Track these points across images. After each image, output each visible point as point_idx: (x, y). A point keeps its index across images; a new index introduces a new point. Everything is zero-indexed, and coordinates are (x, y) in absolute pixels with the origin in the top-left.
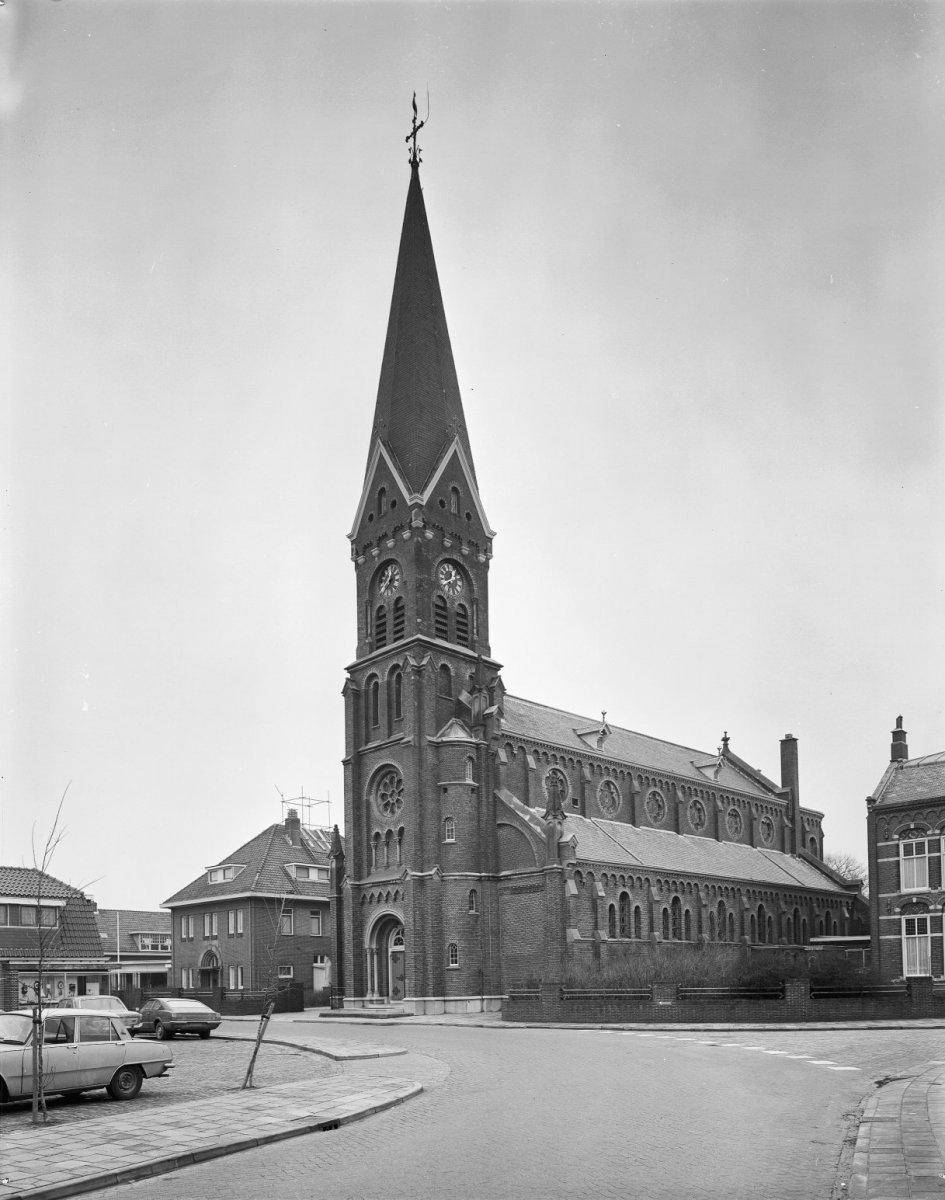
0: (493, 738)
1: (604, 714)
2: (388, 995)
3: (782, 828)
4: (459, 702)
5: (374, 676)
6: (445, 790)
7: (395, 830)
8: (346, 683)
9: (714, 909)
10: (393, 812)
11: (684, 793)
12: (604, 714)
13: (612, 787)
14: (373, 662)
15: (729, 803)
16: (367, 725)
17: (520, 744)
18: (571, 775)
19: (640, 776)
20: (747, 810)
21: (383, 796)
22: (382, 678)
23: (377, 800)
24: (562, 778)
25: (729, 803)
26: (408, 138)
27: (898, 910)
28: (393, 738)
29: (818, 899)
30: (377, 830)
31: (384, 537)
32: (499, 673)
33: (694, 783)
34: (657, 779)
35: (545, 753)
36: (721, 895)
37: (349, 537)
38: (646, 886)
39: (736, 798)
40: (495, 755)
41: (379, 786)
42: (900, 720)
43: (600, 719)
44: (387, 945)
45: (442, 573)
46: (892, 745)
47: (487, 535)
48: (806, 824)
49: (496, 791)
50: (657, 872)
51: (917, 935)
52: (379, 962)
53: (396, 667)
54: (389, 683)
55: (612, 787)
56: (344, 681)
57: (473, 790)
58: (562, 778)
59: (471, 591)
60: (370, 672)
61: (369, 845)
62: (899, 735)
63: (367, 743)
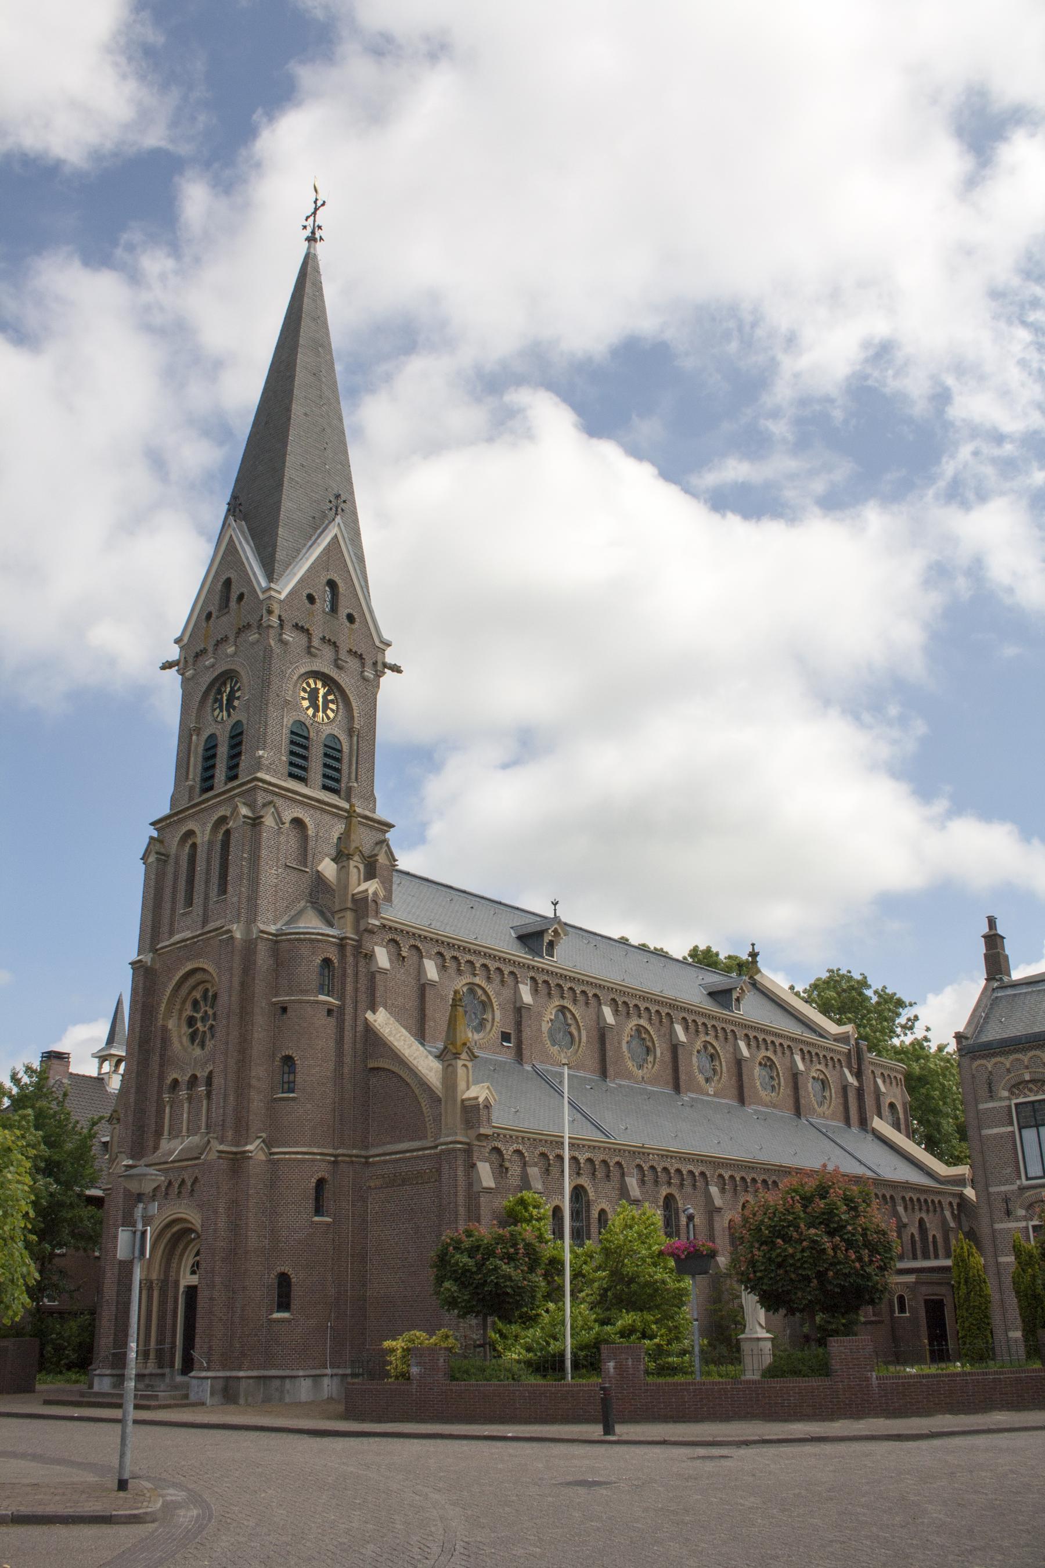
0: (366, 930)
1: (555, 904)
2: (172, 1365)
3: (845, 1088)
4: (319, 877)
5: (191, 833)
6: (284, 1010)
7: (202, 1074)
8: (149, 844)
9: (914, 1230)
10: (202, 1045)
11: (686, 1029)
12: (555, 904)
13: (569, 1016)
14: (907, 1126)
15: (758, 1047)
16: (173, 910)
17: (412, 942)
18: (498, 994)
19: (613, 1000)
20: (787, 1060)
21: (191, 1022)
22: (203, 836)
23: (179, 1026)
24: (484, 998)
25: (758, 1047)
26: (323, 205)
27: (1022, 1212)
28: (211, 926)
29: (903, 1198)
30: (175, 1076)
31: (225, 640)
32: (388, 835)
33: (703, 1015)
34: (643, 1006)
35: (455, 958)
36: (669, 1184)
37: (177, 641)
38: (618, 1174)
39: (769, 1039)
40: (370, 957)
41: (184, 1002)
42: (992, 922)
43: (550, 914)
44: (179, 1268)
45: (304, 690)
46: (986, 955)
47: (378, 643)
48: (879, 1081)
49: (369, 1015)
50: (718, 1163)
51: (132, 1414)
52: (162, 1303)
53: (223, 820)
54: (211, 843)
55: (569, 1016)
56: (147, 840)
57: (330, 1012)
58: (484, 998)
59: (351, 718)
60: (184, 829)
61: (160, 1101)
62: (993, 941)
63: (171, 933)
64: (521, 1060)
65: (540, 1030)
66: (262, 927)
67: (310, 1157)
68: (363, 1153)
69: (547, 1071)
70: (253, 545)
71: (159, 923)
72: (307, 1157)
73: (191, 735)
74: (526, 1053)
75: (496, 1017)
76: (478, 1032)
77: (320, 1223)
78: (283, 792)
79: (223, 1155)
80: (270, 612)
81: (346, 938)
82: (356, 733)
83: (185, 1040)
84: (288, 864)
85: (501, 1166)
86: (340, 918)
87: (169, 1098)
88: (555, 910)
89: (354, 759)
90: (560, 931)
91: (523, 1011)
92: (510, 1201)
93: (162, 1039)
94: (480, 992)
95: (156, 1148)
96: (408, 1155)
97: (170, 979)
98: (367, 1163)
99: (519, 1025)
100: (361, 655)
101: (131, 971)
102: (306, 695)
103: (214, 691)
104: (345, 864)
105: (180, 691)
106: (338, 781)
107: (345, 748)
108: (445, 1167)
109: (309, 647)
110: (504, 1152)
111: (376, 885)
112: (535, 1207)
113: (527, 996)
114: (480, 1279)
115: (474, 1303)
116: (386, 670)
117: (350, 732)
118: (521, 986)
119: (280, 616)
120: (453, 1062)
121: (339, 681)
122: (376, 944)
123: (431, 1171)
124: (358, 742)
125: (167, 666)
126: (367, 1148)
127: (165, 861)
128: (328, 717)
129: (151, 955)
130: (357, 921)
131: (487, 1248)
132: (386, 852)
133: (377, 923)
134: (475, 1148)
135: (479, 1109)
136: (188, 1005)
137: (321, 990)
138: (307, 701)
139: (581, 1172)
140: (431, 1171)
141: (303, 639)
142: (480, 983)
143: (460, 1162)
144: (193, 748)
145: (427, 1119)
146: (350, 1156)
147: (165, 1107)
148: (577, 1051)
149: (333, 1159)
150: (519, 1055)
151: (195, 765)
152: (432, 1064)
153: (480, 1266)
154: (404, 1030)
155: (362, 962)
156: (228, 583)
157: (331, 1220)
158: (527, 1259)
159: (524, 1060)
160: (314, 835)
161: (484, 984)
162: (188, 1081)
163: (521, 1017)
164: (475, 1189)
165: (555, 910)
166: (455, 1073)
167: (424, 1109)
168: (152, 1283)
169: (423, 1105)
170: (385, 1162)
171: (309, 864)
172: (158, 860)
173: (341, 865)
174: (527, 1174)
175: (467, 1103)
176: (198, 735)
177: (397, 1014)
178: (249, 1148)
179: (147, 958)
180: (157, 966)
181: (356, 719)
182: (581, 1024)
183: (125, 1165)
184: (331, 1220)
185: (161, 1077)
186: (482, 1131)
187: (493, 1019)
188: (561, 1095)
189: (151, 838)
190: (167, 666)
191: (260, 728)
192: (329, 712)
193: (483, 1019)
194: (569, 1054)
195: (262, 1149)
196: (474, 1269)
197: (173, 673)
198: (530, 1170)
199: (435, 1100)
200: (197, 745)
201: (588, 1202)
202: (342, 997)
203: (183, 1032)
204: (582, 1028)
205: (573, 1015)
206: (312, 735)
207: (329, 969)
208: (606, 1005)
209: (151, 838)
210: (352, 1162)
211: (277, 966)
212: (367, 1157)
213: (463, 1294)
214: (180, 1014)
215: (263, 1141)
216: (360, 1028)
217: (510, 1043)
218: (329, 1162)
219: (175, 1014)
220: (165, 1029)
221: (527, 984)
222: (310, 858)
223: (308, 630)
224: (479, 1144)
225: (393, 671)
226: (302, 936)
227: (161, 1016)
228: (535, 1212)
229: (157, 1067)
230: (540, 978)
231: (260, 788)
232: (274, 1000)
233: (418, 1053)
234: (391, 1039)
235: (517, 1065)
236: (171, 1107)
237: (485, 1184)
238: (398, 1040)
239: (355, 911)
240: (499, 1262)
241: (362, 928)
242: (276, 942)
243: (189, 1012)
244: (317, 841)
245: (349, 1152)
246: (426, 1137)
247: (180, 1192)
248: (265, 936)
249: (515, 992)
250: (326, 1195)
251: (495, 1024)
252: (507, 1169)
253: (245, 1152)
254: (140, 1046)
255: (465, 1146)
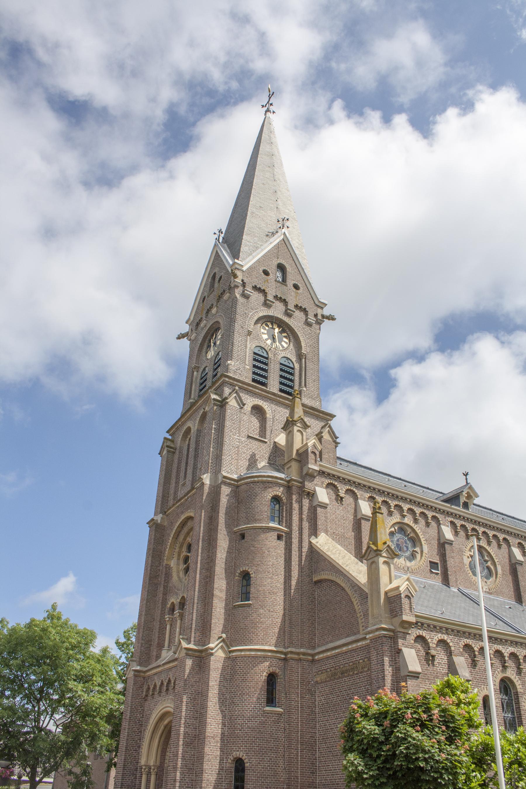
0: (307, 474)
1: (466, 475)
4: (276, 446)
6: (243, 536)
12: (466, 475)
13: (485, 554)
16: (177, 483)
23: (178, 564)
40: (312, 495)
41: (181, 546)
49: (314, 540)
55: (485, 554)
57: (279, 537)
64: (449, 584)
65: (462, 562)
66: (225, 474)
67: (263, 653)
68: (309, 651)
69: (471, 594)
70: (229, 251)
71: (168, 494)
72: (259, 653)
73: (193, 372)
74: (452, 578)
75: (424, 549)
76: (410, 561)
77: (271, 712)
78: (246, 386)
79: (190, 652)
80: (235, 276)
81: (292, 480)
82: (304, 357)
83: (181, 574)
84: (250, 435)
85: (427, 654)
86: (288, 468)
87: (169, 618)
88: (466, 479)
89: (303, 372)
90: (472, 494)
91: (447, 546)
92: (438, 686)
93: (166, 574)
94: (409, 530)
95: (158, 657)
96: (344, 649)
97: (172, 530)
98: (313, 661)
99: (443, 556)
100: (305, 309)
101: (149, 529)
102: (266, 332)
103: (207, 342)
104: (290, 429)
105: (189, 349)
106: (292, 387)
107: (297, 366)
108: (374, 654)
109: (266, 300)
110: (429, 640)
111: (314, 441)
112: (462, 692)
113: (448, 533)
114: (388, 750)
115: (385, 780)
116: (324, 319)
117: (300, 356)
118: (443, 527)
119: (242, 281)
120: (375, 559)
121: (289, 323)
122: (316, 485)
123: (364, 661)
124: (305, 363)
125: (181, 337)
126: (314, 648)
127: (174, 453)
128: (283, 347)
129: (161, 515)
130: (301, 469)
131: (396, 712)
132: (329, 432)
133: (317, 468)
134: (400, 635)
135: (400, 598)
136: (184, 549)
137: (273, 519)
138: (266, 335)
139: (506, 664)
140: (364, 661)
141: (261, 298)
142: (408, 523)
143: (386, 648)
144: (194, 380)
145: (358, 615)
146: (298, 654)
147: (166, 625)
148: (496, 581)
149: (283, 656)
150: (446, 581)
151: (195, 391)
152: (361, 568)
153: (388, 734)
154: (339, 547)
155: (306, 502)
156: (215, 274)
157: (282, 710)
158: (444, 728)
159: (451, 584)
160: (271, 417)
161: (411, 524)
162: (180, 603)
163: (445, 550)
164: (403, 673)
165: (466, 479)
166: (377, 568)
167: (356, 606)
168: (150, 769)
169: (355, 603)
170: (328, 658)
171: (268, 437)
172: (168, 452)
173: (288, 431)
174: (454, 663)
175: (390, 594)
176: (197, 372)
177: (339, 538)
178: (211, 645)
179: (159, 518)
180: (166, 524)
181: (303, 348)
182: (496, 561)
183: (133, 670)
184: (282, 710)
185: (164, 601)
186: (405, 618)
187: (422, 552)
188: (486, 610)
189: (165, 438)
190: (181, 337)
191: (229, 347)
192: (283, 343)
193: (413, 551)
194: (489, 583)
195: (222, 647)
196: (382, 738)
197: (186, 342)
198: (456, 659)
199: (363, 596)
200: (196, 378)
201: (517, 694)
202: (289, 525)
203: (181, 568)
204: (497, 563)
205: (489, 553)
206: (271, 355)
207: (279, 504)
208: (514, 546)
209: (165, 438)
210: (300, 660)
211: (239, 503)
212: (313, 655)
213: (370, 769)
214: (179, 555)
215: (223, 641)
216: (305, 549)
217: (438, 571)
218: (280, 659)
219: (176, 555)
220: (168, 568)
221: (448, 526)
222: (268, 433)
223: (264, 290)
224: (403, 630)
225: (329, 319)
226: (256, 479)
227: (166, 558)
228: (462, 696)
229: (161, 595)
230: (459, 523)
231: (227, 382)
232: (235, 529)
233: (350, 561)
234: (329, 553)
235: (445, 587)
236: (171, 625)
237: (411, 668)
238: (334, 554)
239: (299, 461)
240: (410, 729)
241: (305, 472)
242: (238, 487)
243: (184, 553)
244: (273, 421)
245: (297, 650)
246: (358, 632)
247: (167, 690)
248: (228, 481)
249: (439, 532)
250: (277, 688)
251: (424, 554)
252: (433, 657)
253: (207, 650)
254: (150, 580)
255: (392, 634)
